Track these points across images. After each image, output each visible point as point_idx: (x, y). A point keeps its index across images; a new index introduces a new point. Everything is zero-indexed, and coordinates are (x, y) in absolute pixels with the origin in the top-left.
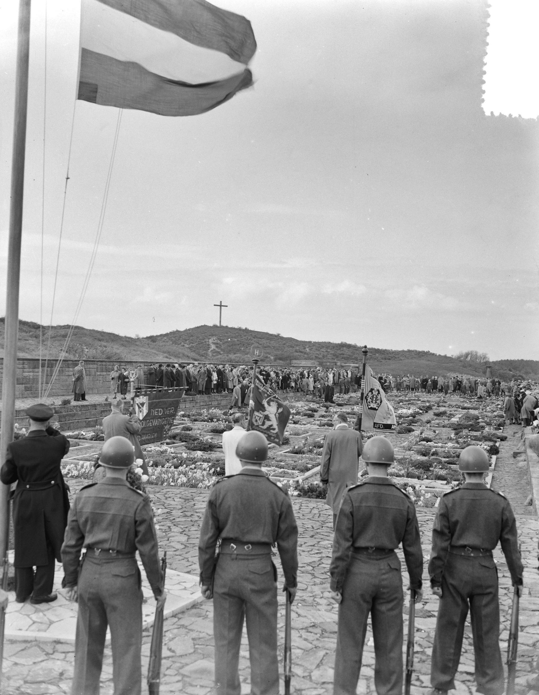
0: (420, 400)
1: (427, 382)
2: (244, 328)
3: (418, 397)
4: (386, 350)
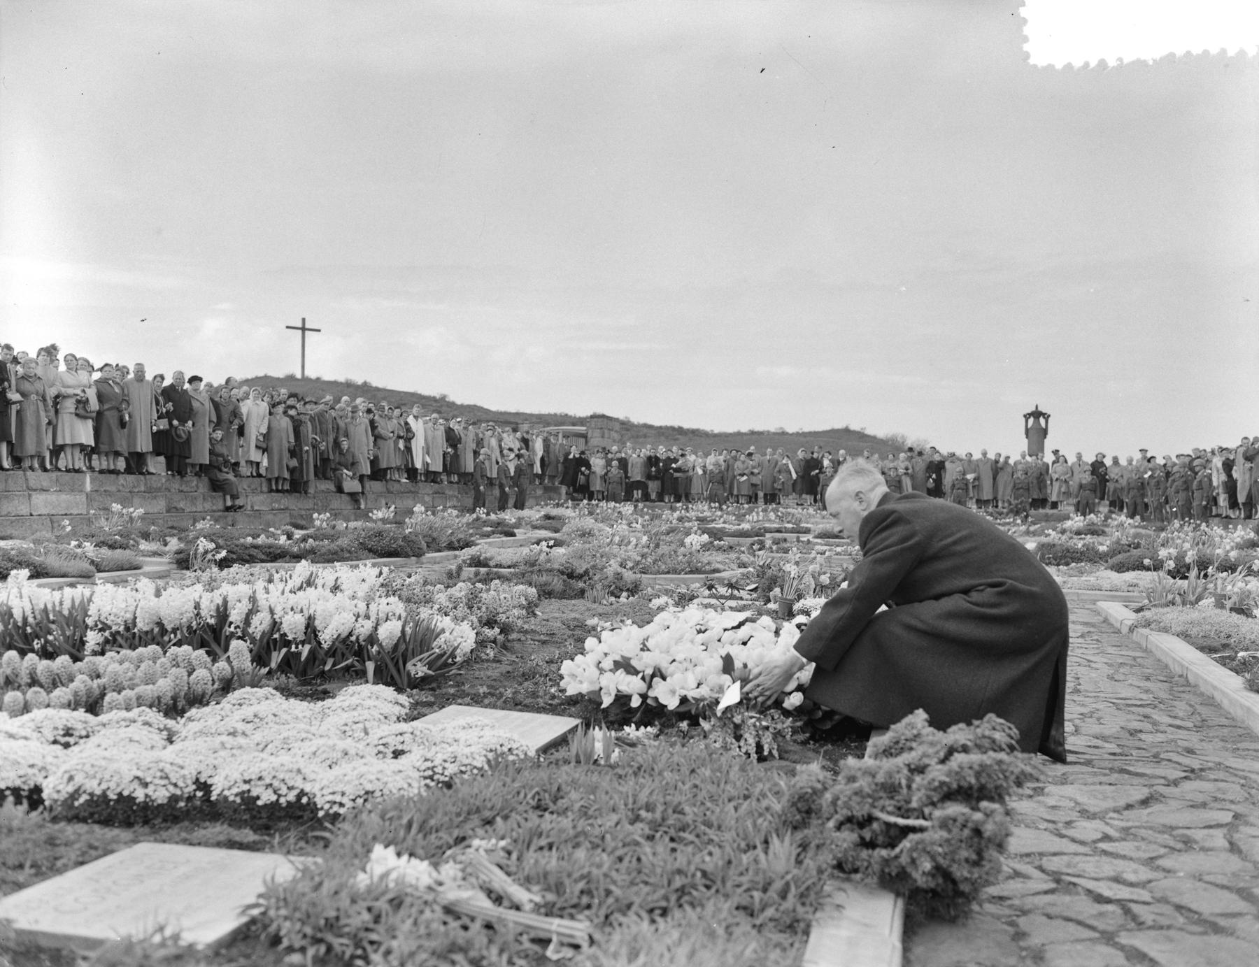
2: (360, 382)
4: (698, 430)
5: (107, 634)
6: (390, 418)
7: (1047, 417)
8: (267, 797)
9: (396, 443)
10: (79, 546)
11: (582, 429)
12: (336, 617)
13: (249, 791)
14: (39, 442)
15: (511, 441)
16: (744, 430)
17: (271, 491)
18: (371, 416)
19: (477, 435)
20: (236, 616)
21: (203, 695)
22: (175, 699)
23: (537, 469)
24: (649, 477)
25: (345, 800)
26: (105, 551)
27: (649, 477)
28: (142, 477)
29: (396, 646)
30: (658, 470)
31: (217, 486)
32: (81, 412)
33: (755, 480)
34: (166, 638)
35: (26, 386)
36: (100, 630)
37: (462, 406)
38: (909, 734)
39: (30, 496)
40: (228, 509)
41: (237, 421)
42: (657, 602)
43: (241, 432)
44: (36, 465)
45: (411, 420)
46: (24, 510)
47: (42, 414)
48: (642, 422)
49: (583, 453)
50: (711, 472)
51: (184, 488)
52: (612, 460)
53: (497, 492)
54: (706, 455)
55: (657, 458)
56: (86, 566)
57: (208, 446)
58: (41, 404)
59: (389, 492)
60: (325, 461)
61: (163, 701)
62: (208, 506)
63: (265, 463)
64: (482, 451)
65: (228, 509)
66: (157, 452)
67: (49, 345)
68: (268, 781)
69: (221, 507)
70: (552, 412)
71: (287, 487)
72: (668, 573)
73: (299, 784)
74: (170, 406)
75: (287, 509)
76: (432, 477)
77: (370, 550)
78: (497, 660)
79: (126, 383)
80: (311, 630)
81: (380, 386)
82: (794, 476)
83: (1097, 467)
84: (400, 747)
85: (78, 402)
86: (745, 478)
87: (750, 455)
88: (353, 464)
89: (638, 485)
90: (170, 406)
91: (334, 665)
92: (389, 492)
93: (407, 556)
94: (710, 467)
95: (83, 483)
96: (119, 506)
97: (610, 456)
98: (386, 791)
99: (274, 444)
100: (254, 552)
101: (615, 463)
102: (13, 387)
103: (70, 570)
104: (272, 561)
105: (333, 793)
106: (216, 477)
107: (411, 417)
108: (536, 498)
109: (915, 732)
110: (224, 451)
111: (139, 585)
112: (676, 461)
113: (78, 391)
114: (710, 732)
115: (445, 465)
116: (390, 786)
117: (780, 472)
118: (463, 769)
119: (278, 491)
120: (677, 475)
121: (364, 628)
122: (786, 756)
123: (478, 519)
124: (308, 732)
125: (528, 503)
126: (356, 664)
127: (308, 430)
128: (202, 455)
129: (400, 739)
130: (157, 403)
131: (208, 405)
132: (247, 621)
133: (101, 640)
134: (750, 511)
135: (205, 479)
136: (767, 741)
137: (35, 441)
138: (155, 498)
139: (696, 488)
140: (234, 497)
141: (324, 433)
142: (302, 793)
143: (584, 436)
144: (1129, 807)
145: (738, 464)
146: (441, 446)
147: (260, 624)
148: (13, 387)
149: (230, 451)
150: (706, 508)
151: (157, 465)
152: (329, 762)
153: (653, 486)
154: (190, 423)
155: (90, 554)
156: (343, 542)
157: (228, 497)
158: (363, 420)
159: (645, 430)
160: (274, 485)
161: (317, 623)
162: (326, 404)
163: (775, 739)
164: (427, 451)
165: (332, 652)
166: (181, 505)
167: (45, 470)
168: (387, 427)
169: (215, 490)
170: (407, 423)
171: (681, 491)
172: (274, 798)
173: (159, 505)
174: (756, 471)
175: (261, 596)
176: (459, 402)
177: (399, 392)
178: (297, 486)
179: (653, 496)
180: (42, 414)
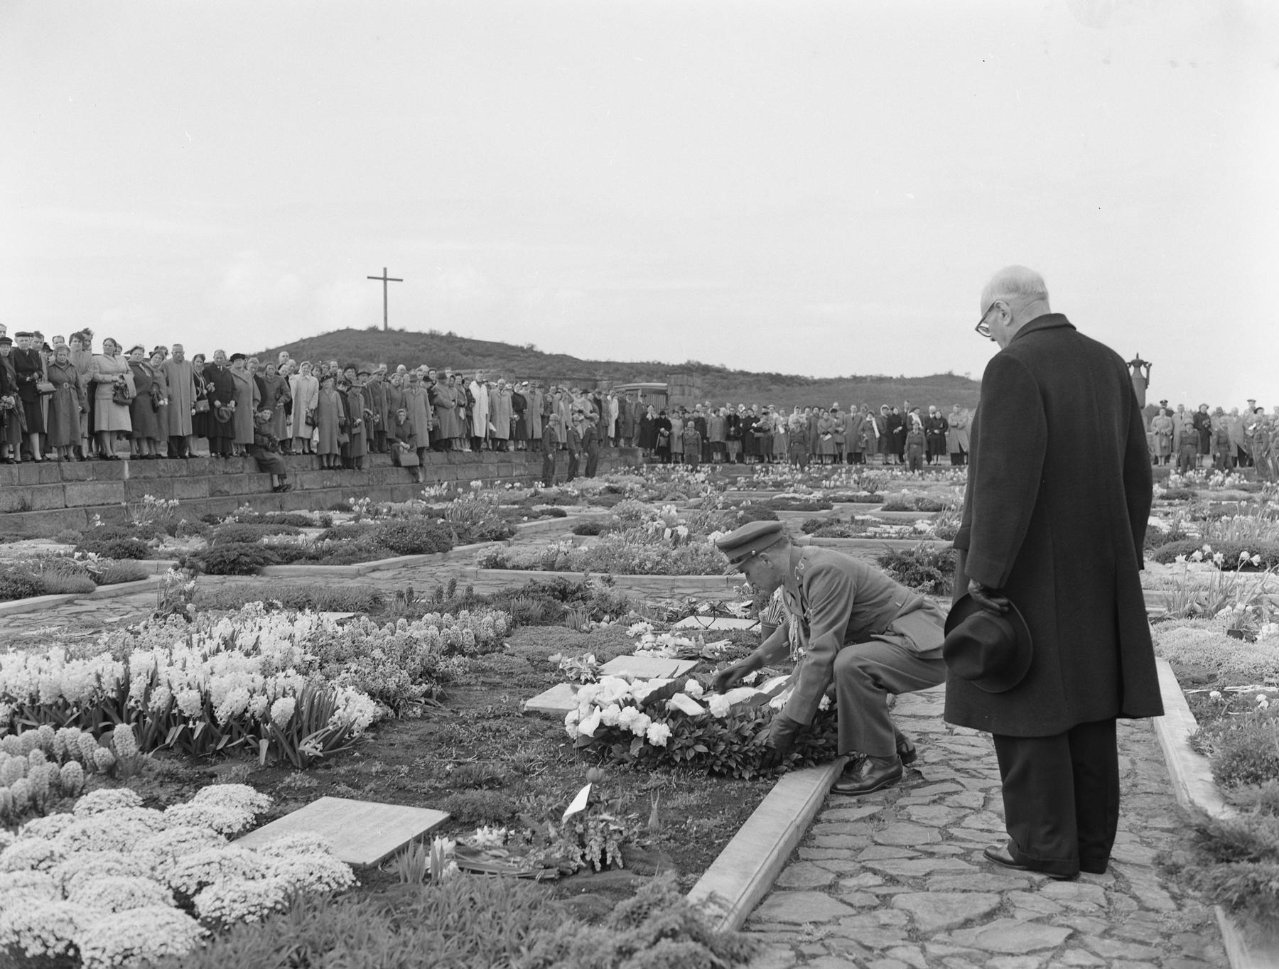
0: (880, 500)
1: (668, 425)
2: (445, 333)
3: (873, 485)
4: (797, 377)
5: (14, 706)
6: (450, 386)
7: (1149, 367)
8: (34, 949)
9: (457, 412)
10: (83, 558)
11: (661, 385)
12: (230, 694)
13: (18, 942)
14: (74, 430)
15: (582, 402)
16: (847, 375)
17: (322, 468)
18: (429, 384)
19: (545, 398)
20: (136, 689)
21: (73, 788)
22: (33, 798)
23: (612, 432)
24: (728, 437)
25: (104, 958)
26: (110, 562)
27: (728, 437)
28: (184, 461)
29: (290, 722)
30: (738, 430)
31: (264, 466)
32: (120, 398)
33: (839, 439)
34: (68, 712)
35: (58, 374)
36: (7, 702)
37: (550, 355)
38: (653, 898)
39: (64, 487)
40: (275, 490)
41: (283, 398)
42: (636, 628)
43: (288, 408)
44: (72, 455)
45: (473, 387)
46: (59, 502)
47: (76, 402)
48: (738, 369)
49: (662, 413)
50: (793, 431)
51: (229, 469)
52: (689, 420)
53: (567, 458)
54: (787, 414)
55: (736, 417)
56: (86, 580)
57: (252, 424)
58: (74, 393)
59: (450, 463)
60: (380, 433)
61: (19, 803)
62: (254, 487)
63: (316, 438)
64: (552, 416)
65: (275, 490)
66: (198, 433)
67: (81, 329)
68: (36, 932)
69: (268, 487)
70: (645, 361)
71: (338, 463)
72: (688, 573)
73: (68, 934)
74: (211, 386)
75: (339, 486)
76: (498, 444)
77: (392, 548)
78: (425, 717)
79: (165, 365)
80: (207, 705)
81: (466, 336)
82: (877, 435)
83: (1200, 419)
84: (204, 879)
85: (116, 388)
86: (829, 436)
87: (834, 411)
88: (410, 436)
89: (722, 447)
90: (211, 386)
91: (230, 741)
92: (450, 463)
93: (431, 552)
94: (792, 426)
95: (122, 470)
96: (152, 498)
97: (687, 416)
98: (145, 948)
99: (325, 419)
100: (268, 554)
101: (691, 423)
102: (45, 376)
103: (69, 586)
104: (287, 563)
105: (94, 949)
106: (265, 454)
107: (474, 383)
108: (612, 462)
109: (659, 896)
110: (272, 431)
111: (51, 654)
112: (757, 420)
113: (116, 377)
114: (556, 839)
115: (511, 432)
116: (150, 943)
117: (863, 430)
118: (252, 909)
119: (330, 468)
120: (757, 435)
121: (259, 703)
122: (630, 864)
123: (537, 493)
124: (117, 861)
125: (600, 468)
126: (251, 742)
127: (360, 403)
128: (247, 435)
129: (207, 868)
130: (197, 383)
131: (252, 383)
132: (147, 695)
133: (9, 712)
134: (834, 471)
135: (251, 459)
136: (612, 848)
137: (72, 427)
138: (197, 482)
139: (780, 446)
140: (282, 477)
141: (377, 406)
142: (71, 945)
143: (663, 392)
144: (967, 923)
145: (821, 422)
146: (507, 414)
147: (159, 698)
148: (45, 376)
149: (276, 429)
150: (787, 470)
151: (200, 448)
152: (113, 905)
153: (734, 447)
154: (233, 403)
155: (92, 567)
156: (363, 540)
157: (276, 477)
158: (422, 387)
159: (742, 378)
160: (324, 462)
161: (212, 699)
162: (379, 374)
163: (620, 847)
164: (491, 418)
165: (228, 729)
166: (226, 488)
167: (82, 459)
168: (447, 395)
169: (262, 471)
170: (468, 391)
171: (762, 451)
172: (42, 950)
173: (202, 490)
174: (840, 429)
175: (162, 670)
176: (547, 352)
177: (485, 343)
178: (348, 460)
179: (733, 457)
180: (76, 402)
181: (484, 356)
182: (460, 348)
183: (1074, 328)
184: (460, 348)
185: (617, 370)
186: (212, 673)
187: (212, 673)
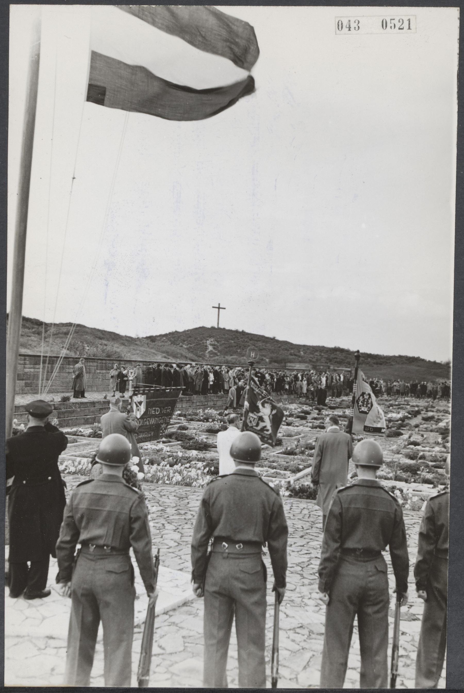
2: (241, 330)
181: (257, 341)
182: (248, 337)
183: (8, 457)
184: (248, 337)
185: (308, 349)
186: (340, 189)
187: (340, 189)
